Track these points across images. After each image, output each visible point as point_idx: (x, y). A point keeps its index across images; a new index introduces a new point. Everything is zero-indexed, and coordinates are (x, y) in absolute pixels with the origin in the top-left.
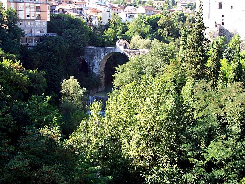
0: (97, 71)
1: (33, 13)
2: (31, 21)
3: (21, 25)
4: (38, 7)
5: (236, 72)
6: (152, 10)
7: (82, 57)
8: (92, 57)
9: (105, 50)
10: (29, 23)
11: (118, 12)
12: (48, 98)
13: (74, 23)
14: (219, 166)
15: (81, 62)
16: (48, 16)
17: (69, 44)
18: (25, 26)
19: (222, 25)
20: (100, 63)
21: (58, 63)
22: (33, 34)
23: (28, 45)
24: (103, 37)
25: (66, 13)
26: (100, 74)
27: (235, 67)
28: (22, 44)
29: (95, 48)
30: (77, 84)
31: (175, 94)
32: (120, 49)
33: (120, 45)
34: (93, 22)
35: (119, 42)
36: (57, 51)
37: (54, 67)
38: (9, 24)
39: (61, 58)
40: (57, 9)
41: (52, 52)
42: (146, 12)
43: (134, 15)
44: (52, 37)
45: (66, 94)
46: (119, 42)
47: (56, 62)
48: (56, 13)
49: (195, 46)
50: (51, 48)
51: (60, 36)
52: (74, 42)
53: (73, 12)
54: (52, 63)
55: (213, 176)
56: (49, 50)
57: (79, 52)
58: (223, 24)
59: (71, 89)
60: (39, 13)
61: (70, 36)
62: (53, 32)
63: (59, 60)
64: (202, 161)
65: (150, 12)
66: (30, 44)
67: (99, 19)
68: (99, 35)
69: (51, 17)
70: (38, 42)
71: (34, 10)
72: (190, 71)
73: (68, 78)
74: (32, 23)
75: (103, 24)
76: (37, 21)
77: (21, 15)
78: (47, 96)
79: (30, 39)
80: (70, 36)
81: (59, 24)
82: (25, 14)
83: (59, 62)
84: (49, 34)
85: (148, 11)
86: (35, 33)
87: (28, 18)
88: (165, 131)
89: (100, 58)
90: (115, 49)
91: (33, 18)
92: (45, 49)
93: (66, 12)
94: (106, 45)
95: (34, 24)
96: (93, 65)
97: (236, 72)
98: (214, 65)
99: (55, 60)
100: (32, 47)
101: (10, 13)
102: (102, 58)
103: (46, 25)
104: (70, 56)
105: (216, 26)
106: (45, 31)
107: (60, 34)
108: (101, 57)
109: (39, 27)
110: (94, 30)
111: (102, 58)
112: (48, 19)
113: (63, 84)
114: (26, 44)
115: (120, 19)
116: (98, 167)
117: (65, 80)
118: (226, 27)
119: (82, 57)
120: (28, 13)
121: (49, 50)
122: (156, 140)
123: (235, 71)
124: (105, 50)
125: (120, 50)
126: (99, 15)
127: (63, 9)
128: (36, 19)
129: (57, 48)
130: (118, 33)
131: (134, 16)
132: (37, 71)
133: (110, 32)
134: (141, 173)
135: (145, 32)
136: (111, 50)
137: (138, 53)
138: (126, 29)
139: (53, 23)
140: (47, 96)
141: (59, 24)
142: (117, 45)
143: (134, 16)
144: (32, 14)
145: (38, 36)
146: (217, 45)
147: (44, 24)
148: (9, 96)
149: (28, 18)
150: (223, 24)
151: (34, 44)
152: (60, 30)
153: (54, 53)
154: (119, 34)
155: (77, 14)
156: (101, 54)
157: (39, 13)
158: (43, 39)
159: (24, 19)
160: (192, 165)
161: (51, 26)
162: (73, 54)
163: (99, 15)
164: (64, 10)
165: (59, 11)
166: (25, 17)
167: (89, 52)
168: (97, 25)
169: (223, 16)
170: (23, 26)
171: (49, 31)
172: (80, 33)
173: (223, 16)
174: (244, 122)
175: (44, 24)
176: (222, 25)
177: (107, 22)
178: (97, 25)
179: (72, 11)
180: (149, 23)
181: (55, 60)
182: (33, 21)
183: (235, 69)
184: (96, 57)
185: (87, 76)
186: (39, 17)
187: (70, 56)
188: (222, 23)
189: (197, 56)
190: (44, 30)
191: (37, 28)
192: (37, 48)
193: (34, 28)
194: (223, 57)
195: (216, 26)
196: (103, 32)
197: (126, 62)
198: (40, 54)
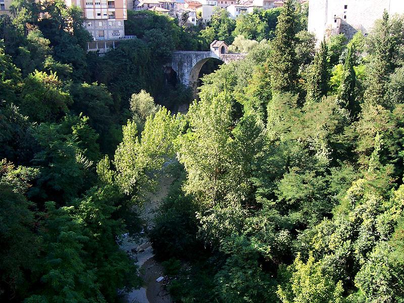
0: (187, 83)
1: (105, 11)
2: (103, 21)
3: (89, 27)
4: (112, 3)
5: (347, 82)
6: (272, 2)
7: (168, 65)
8: (181, 65)
9: (197, 56)
10: (100, 24)
11: (226, 5)
12: (85, 119)
13: (158, 21)
14: (296, 207)
15: (169, 72)
16: (125, 14)
17: (151, 49)
18: (95, 27)
19: (344, 20)
20: (190, 72)
21: (137, 73)
22: (106, 38)
23: (98, 51)
24: (199, 38)
25: (152, 10)
26: (192, 86)
27: (346, 75)
28: (92, 50)
29: (184, 52)
30: (151, 99)
31: (261, 112)
32: (216, 54)
33: (216, 48)
34: (190, 19)
35: (214, 44)
36: (134, 58)
37: (131, 78)
38: (74, 26)
39: (140, 67)
40: (140, 5)
41: (128, 60)
42: (265, 4)
43: (247, 8)
44: (129, 41)
45: (136, 112)
46: (214, 44)
47: (134, 71)
48: (139, 10)
49: (282, 47)
50: (127, 55)
51: (140, 40)
52: (158, 46)
53: (162, 7)
54: (128, 73)
55: (288, 220)
56: (124, 56)
57: (165, 58)
58: (345, 17)
59: (142, 106)
60: (113, 10)
61: (152, 38)
62: (133, 34)
63: (138, 70)
64: (272, 200)
65: (270, 4)
66: (102, 50)
67: (198, 16)
68: (194, 36)
69: (130, 14)
70: (112, 47)
71: (106, 6)
72: (276, 81)
73: (138, 92)
74: (104, 23)
75: (204, 21)
76: (110, 21)
77: (90, 14)
78: (84, 117)
79: (101, 44)
80: (152, 38)
81: (139, 23)
82: (94, 13)
83: (138, 72)
84: (127, 36)
85: (267, 4)
86: (110, 36)
87: (99, 17)
88: (231, 161)
89: (191, 66)
90: (209, 54)
91: (106, 17)
92: (120, 56)
93: (151, 7)
94: (202, 49)
95: (107, 24)
96: (183, 75)
97: (347, 82)
98: (319, 73)
99: (132, 69)
100: (104, 54)
101: (74, 13)
102: (194, 65)
103: (123, 26)
104: (152, 64)
105: (335, 21)
106: (122, 33)
107: (140, 36)
108: (192, 64)
109: (114, 27)
110: (188, 29)
111: (194, 65)
112: (125, 17)
113: (132, 100)
114: (96, 50)
115: (227, 15)
116: (72, 207)
117: (133, 95)
118: (349, 21)
119: (168, 65)
120: (98, 11)
121: (124, 56)
122: (221, 173)
123: (345, 81)
124: (197, 56)
125: (215, 55)
126: (200, 10)
127: (148, 4)
128: (109, 18)
129: (135, 54)
130: (220, 33)
131: (246, 10)
132: (97, 84)
133: (207, 32)
134: (196, 214)
135: (259, 31)
136: (204, 55)
137: (238, 58)
138: (232, 28)
139: (133, 22)
140: (84, 117)
141: (139, 23)
142: (212, 49)
143: (246, 10)
144: (104, 11)
145: (111, 41)
146: (322, 47)
147: (120, 25)
148: (26, 118)
149: (99, 17)
150: (345, 17)
151: (106, 49)
152: (142, 31)
153: (131, 60)
154: (222, 34)
155: (165, 10)
156: (191, 61)
157: (113, 10)
158: (118, 43)
159: (93, 18)
160: (260, 206)
161: (129, 26)
162: (157, 61)
163: (200, 10)
164: (150, 6)
165: (143, 7)
166: (95, 17)
167: (178, 58)
168: (195, 23)
169: (346, 7)
170: (93, 28)
171: (127, 33)
172: (165, 33)
173: (346, 7)
174: (332, 150)
175: (120, 24)
176: (344, 20)
177: (210, 19)
178: (195, 23)
179: (161, 6)
180: (267, 19)
181: (132, 69)
182: (106, 21)
183: (346, 78)
184: (186, 64)
185: (176, 89)
186: (113, 15)
187: (152, 64)
188: (344, 17)
189: (284, 62)
190: (120, 31)
191: (111, 29)
192: (109, 55)
193: (108, 30)
194: (340, 62)
195: (335, 21)
196: (198, 32)
197: (215, 71)
198: (112, 63)
